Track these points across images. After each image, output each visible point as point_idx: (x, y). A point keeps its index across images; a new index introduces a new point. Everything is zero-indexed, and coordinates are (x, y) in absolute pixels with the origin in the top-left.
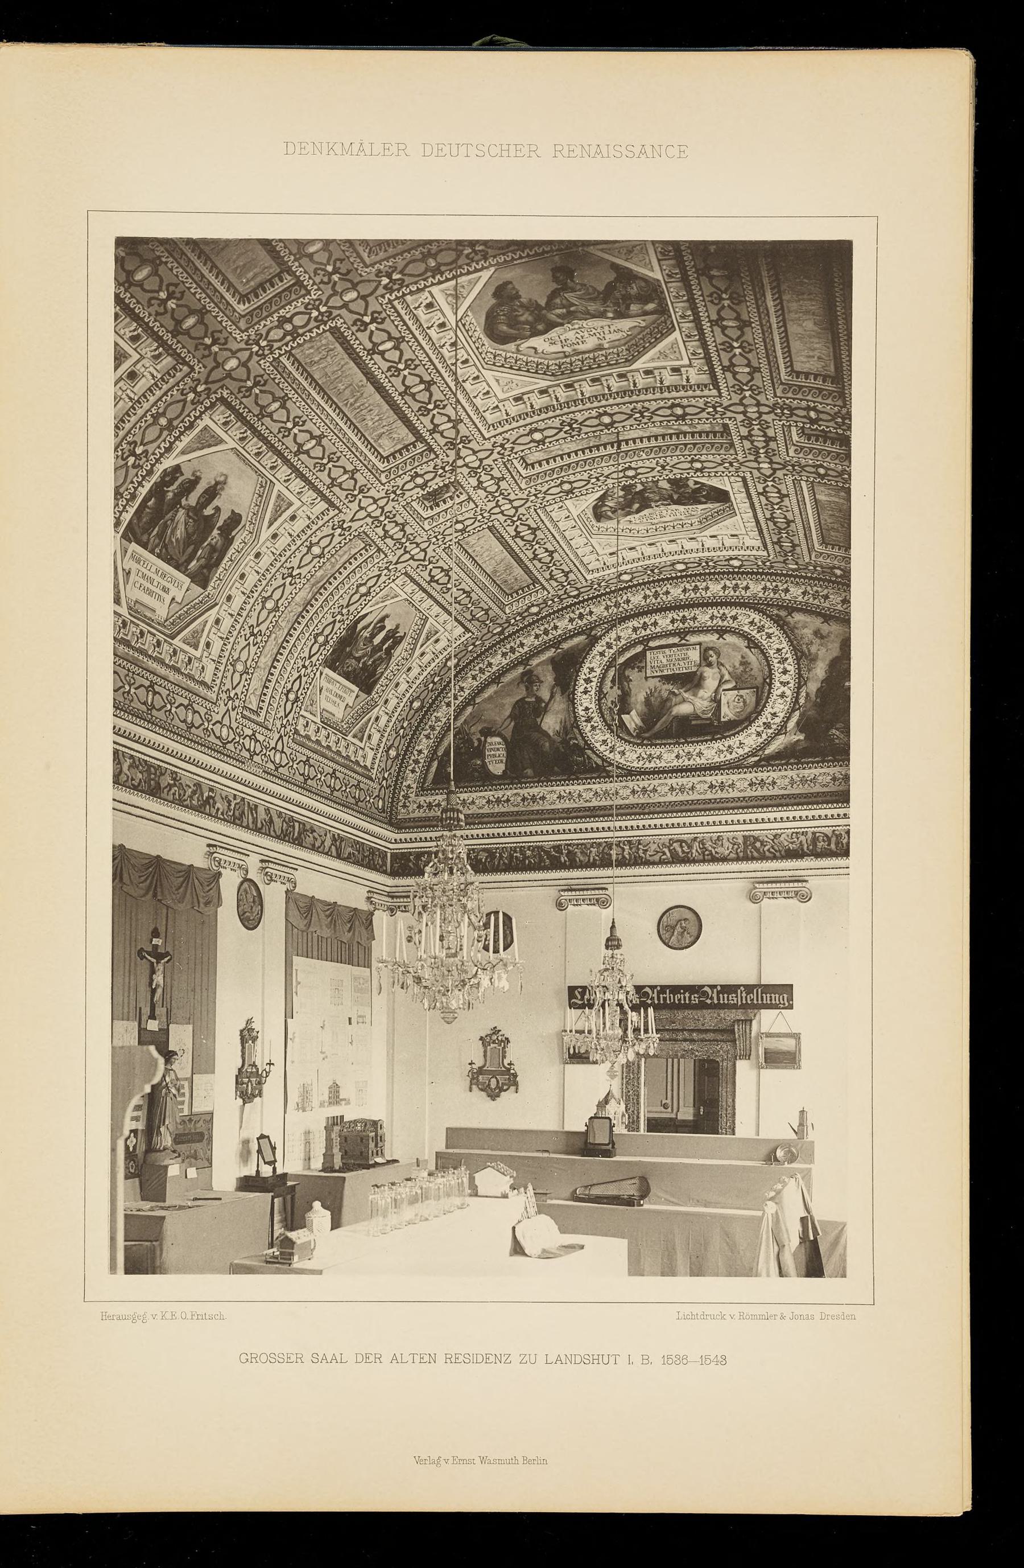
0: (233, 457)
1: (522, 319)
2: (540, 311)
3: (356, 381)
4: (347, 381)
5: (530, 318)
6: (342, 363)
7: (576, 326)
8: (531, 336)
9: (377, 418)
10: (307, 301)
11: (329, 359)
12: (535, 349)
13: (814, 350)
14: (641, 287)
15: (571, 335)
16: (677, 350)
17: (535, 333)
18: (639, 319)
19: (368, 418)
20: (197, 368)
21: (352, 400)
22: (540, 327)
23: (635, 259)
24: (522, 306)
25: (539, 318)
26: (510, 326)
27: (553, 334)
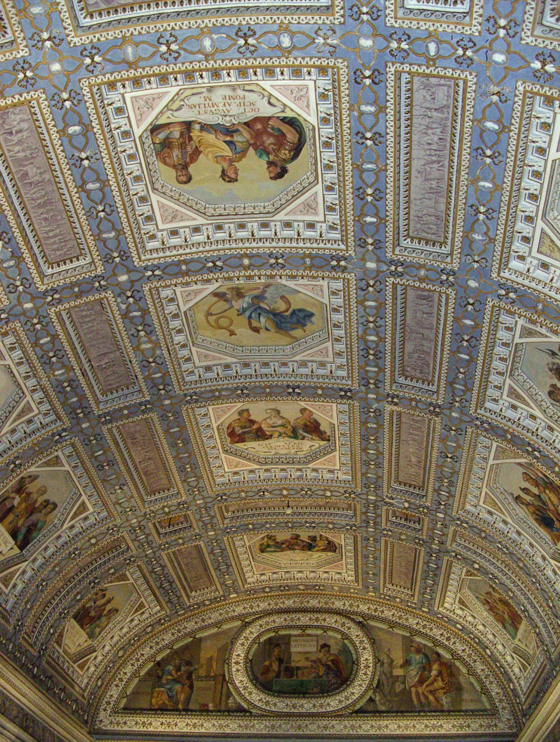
0: (550, 216)
1: (271, 140)
2: (255, 143)
3: (420, 179)
4: (428, 185)
5: (265, 138)
6: (418, 202)
7: (228, 119)
8: (269, 118)
9: (430, 131)
10: (398, 280)
11: (425, 212)
12: (269, 103)
13: (19, 142)
14: (169, 157)
15: (234, 110)
16: (138, 112)
17: (265, 120)
18: (173, 120)
19: (436, 138)
20: (491, 304)
21: (435, 166)
22: (259, 126)
23: (170, 211)
24: (268, 154)
25: (258, 135)
26: (283, 135)
27: (250, 116)
